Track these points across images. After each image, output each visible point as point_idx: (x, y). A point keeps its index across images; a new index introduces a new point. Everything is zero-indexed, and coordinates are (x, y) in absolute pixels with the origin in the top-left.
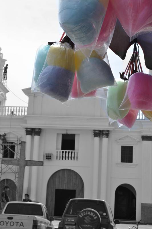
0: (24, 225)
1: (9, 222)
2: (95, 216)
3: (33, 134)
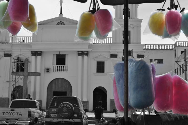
0: (22, 114)
1: (11, 113)
2: (70, 107)
3: (37, 55)
